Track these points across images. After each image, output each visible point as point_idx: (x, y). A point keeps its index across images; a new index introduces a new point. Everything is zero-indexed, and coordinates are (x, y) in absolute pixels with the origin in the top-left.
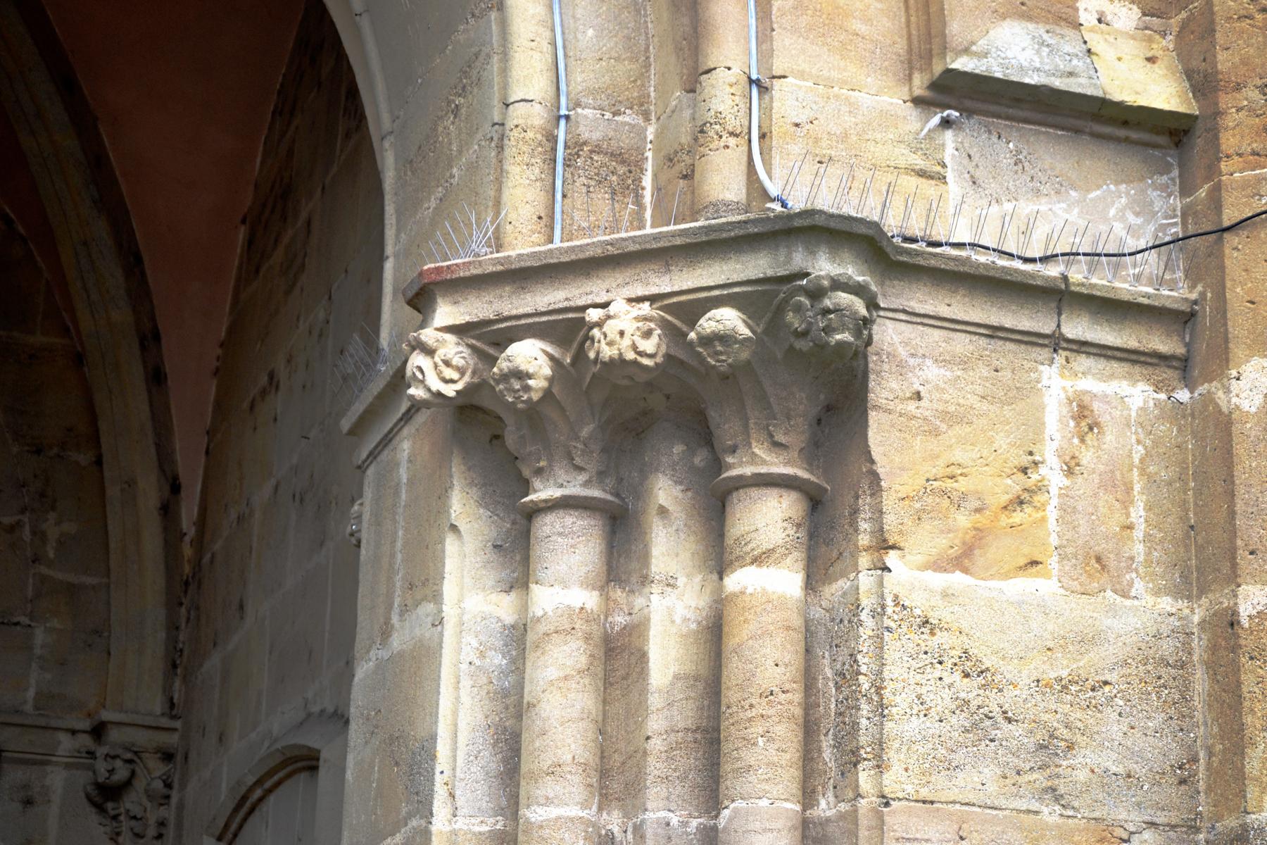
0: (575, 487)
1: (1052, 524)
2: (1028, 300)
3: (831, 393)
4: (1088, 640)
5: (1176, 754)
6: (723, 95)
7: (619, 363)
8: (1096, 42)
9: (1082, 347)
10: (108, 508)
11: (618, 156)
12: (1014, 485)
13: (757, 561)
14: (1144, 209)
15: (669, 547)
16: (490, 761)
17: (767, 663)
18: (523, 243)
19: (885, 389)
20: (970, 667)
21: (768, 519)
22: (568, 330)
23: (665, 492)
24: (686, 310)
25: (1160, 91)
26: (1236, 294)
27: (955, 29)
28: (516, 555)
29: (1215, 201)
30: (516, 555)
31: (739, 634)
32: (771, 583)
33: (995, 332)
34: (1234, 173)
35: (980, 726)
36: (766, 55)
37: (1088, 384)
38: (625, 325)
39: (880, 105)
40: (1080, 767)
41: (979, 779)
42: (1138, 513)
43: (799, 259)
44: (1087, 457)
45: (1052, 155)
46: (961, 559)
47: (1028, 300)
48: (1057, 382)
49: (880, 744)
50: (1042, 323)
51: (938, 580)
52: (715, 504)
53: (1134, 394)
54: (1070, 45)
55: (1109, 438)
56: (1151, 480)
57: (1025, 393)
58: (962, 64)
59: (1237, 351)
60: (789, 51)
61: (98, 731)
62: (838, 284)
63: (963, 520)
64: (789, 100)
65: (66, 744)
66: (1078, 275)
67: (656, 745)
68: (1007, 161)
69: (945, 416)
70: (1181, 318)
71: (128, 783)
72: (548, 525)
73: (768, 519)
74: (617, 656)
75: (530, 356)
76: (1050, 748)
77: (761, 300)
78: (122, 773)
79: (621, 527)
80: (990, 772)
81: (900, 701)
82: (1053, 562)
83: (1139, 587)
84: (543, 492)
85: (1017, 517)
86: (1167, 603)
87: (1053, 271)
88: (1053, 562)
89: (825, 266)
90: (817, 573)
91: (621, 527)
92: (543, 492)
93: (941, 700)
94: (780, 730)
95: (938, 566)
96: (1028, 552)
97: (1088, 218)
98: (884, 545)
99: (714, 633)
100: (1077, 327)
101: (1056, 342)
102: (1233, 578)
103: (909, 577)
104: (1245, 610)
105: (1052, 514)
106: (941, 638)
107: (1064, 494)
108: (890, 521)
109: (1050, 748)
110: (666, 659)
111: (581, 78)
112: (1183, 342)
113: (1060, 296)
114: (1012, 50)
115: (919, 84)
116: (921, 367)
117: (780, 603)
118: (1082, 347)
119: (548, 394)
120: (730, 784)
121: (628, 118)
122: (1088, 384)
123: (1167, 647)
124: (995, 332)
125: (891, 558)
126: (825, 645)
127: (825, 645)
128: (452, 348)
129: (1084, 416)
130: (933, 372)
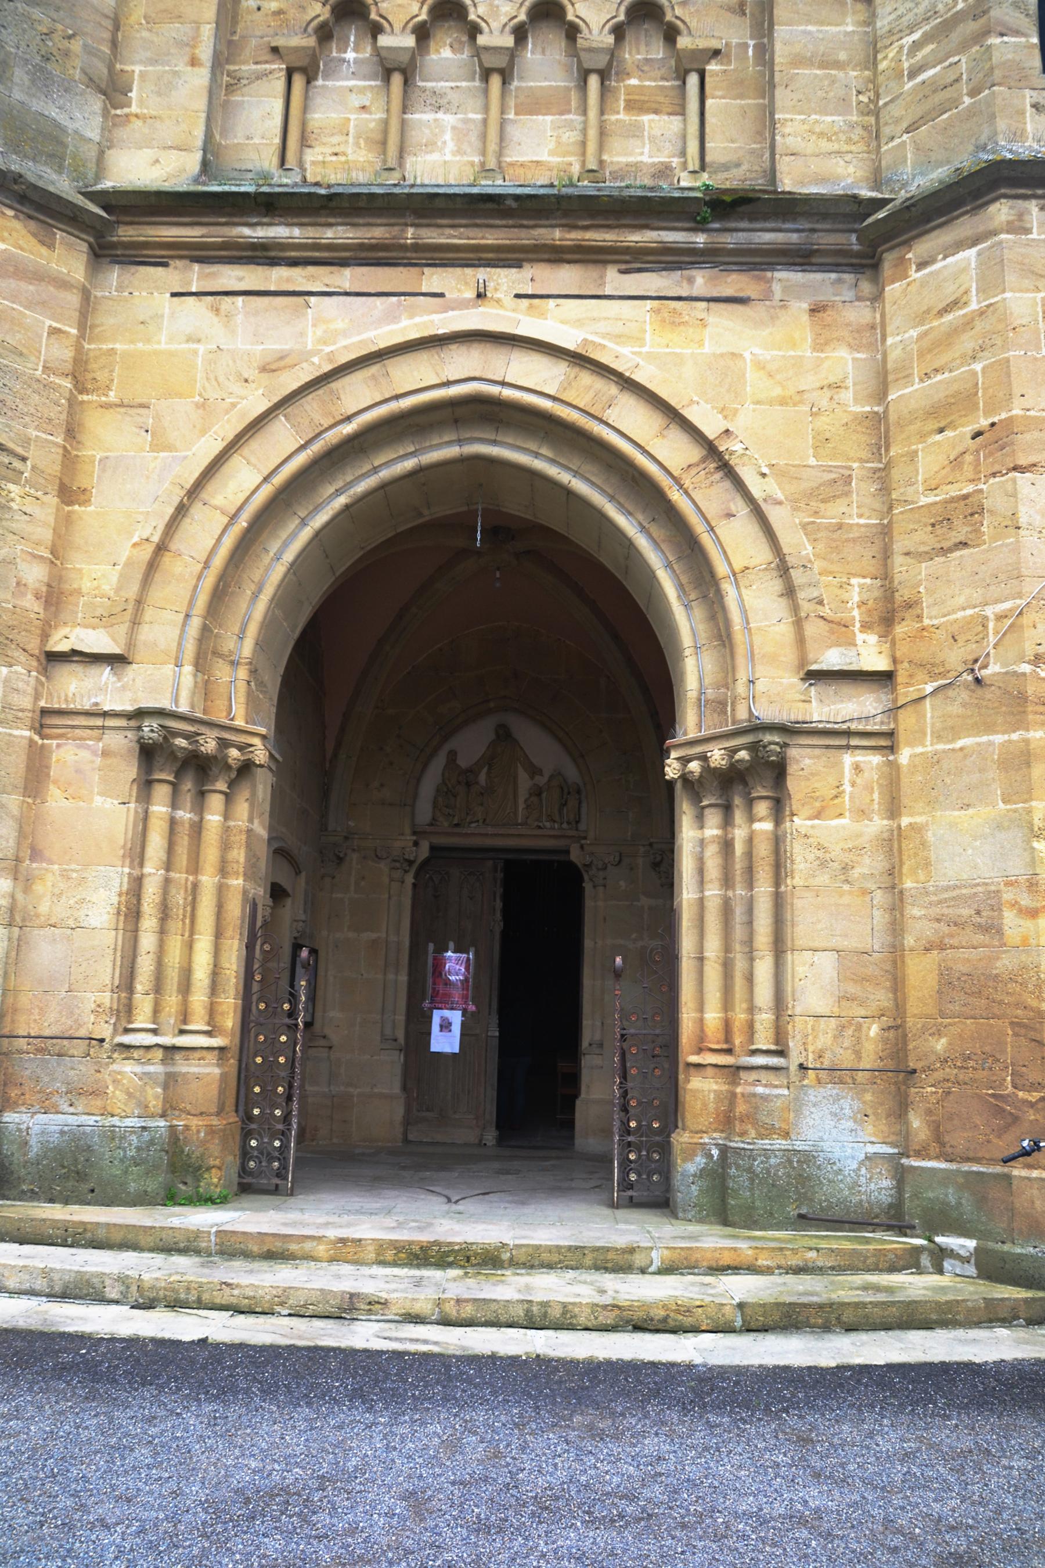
0: (713, 801)
1: (847, 802)
2: (839, 736)
3: (778, 772)
4: (859, 835)
5: (888, 866)
6: (741, 688)
7: (715, 768)
8: (861, 650)
9: (857, 747)
10: (44, 1299)
11: (720, 703)
12: (834, 792)
13: (759, 820)
14: (878, 700)
15: (739, 816)
16: (697, 878)
17: (763, 850)
18: (692, 735)
19: (792, 769)
20: (820, 847)
21: (762, 808)
22: (704, 758)
23: (737, 801)
24: (734, 751)
25: (882, 664)
26: (901, 728)
27: (811, 656)
28: (700, 820)
29: (895, 700)
30: (700, 820)
31: (755, 841)
32: (766, 826)
33: (828, 747)
34: (901, 689)
35: (823, 864)
36: (753, 673)
37: (859, 758)
38: (717, 756)
39: (792, 681)
40: (856, 873)
41: (823, 879)
42: (876, 796)
43: (760, 736)
44: (859, 781)
45: (847, 688)
46: (818, 816)
47: (839, 736)
48: (848, 759)
49: (792, 871)
50: (844, 742)
51: (809, 823)
52: (750, 802)
53: (876, 759)
54: (853, 653)
55: (866, 774)
56: (880, 786)
57: (839, 764)
58: (814, 667)
59: (901, 745)
60: (761, 670)
61: (651, 845)
62: (770, 743)
63: (817, 804)
64: (760, 686)
65: (642, 849)
66: (854, 726)
67: (738, 872)
68: (832, 693)
69: (812, 774)
70: (891, 734)
71: (661, 861)
72: (707, 811)
73: (762, 808)
74: (727, 846)
75: (694, 766)
76: (845, 868)
77: (753, 747)
78: (659, 859)
79: (727, 809)
80: (827, 877)
81: (798, 859)
82: (847, 814)
83: (876, 818)
84: (705, 803)
85: (836, 801)
86: (885, 822)
87: (844, 726)
88: (847, 814)
89: (768, 738)
90: (778, 821)
91: (727, 809)
92: (705, 803)
93: (811, 857)
94: (766, 868)
95: (810, 819)
96: (839, 811)
97: (858, 707)
98: (793, 815)
99: (750, 841)
100: (855, 742)
101: (848, 747)
102: (900, 815)
103: (799, 822)
104: (903, 825)
105: (847, 798)
106: (811, 840)
107: (851, 793)
108: (794, 807)
109: (845, 868)
110: (739, 848)
111: (707, 681)
112: (887, 741)
113: (848, 733)
114: (833, 659)
115: (802, 675)
116: (805, 763)
117: (766, 832)
118: (857, 747)
119: (701, 776)
120: (755, 884)
121: (723, 690)
122: (859, 758)
123: (885, 835)
124: (828, 747)
125: (795, 818)
126: (778, 841)
127: (778, 841)
128: (676, 765)
129: (857, 768)
130: (807, 761)
